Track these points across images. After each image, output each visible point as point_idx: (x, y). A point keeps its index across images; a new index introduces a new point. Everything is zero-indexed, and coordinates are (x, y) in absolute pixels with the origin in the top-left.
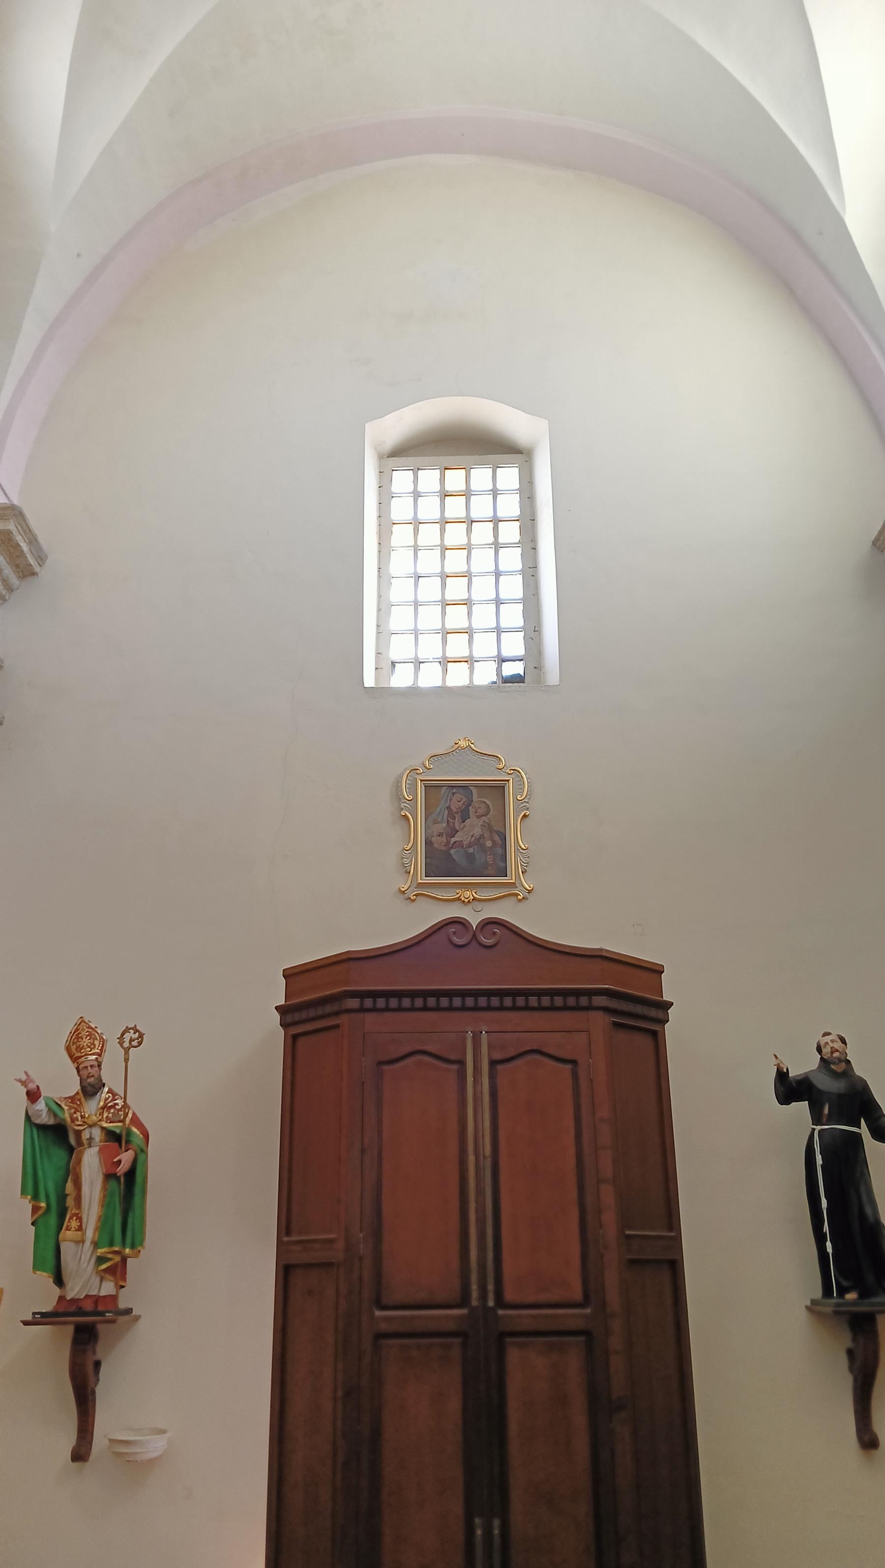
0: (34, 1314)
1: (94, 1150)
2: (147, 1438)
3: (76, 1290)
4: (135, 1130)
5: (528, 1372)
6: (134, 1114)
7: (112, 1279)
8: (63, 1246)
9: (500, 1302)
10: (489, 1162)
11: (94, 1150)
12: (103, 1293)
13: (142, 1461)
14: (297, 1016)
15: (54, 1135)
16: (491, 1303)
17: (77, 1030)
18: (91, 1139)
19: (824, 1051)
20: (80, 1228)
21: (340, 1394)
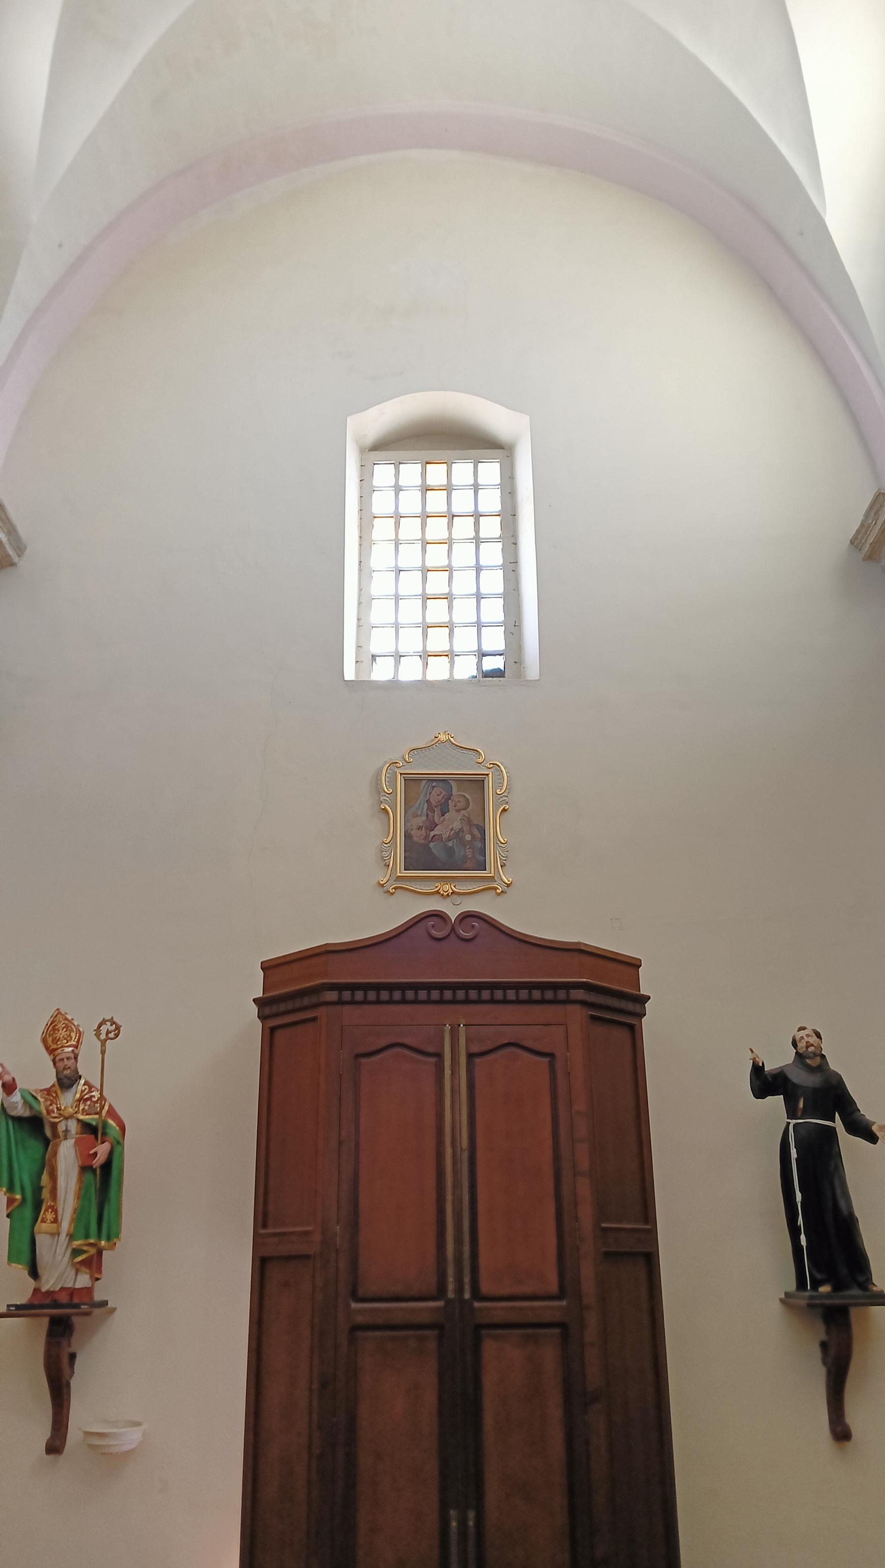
0: (8, 1306)
3: (52, 1282)
6: (110, 1106)
7: (88, 1271)
8: (39, 1239)
9: (477, 1294)
10: (465, 1156)
12: (79, 1285)
13: (117, 1453)
14: (274, 1009)
16: (467, 1296)
18: (66, 1131)
19: (800, 1045)
20: (55, 1221)
21: (315, 1386)
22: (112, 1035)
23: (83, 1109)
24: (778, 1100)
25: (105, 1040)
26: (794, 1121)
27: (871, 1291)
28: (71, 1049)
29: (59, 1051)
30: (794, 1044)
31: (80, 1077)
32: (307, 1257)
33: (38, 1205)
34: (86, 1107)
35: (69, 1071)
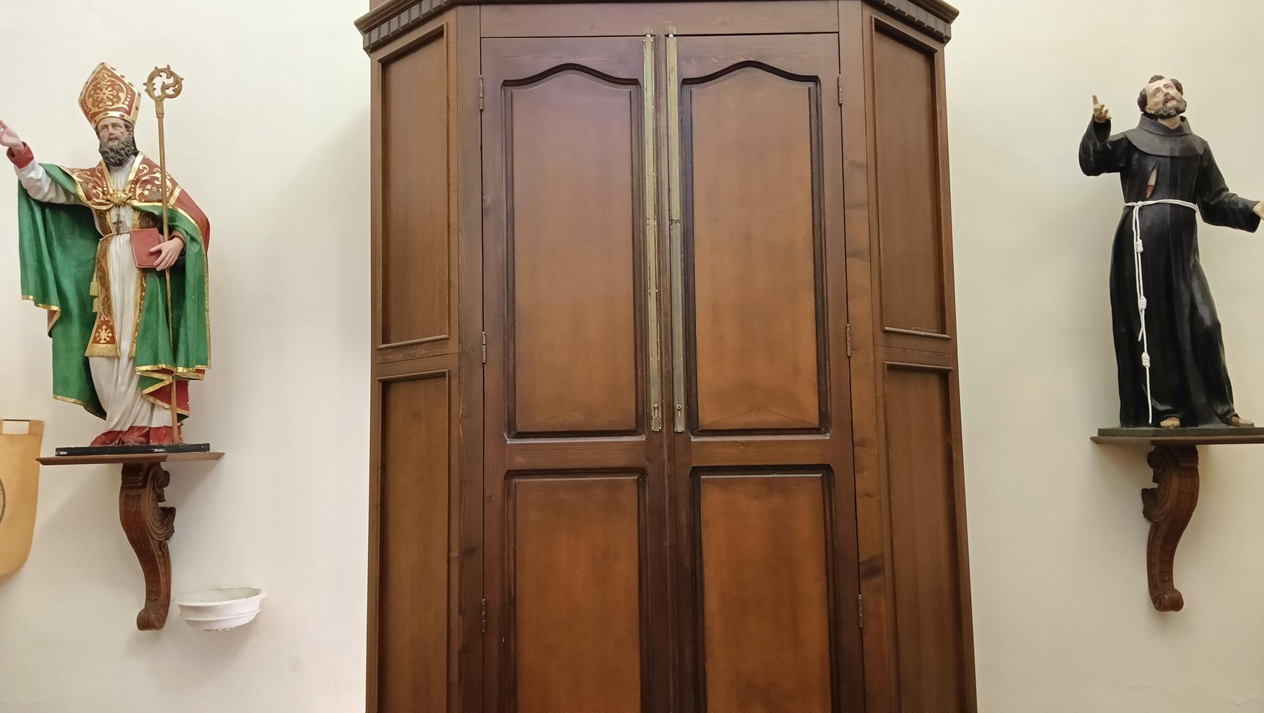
0: (58, 450)
1: (125, 238)
2: (224, 603)
3: (116, 420)
4: (180, 211)
5: (733, 523)
6: (183, 192)
7: (167, 406)
8: (93, 363)
9: (693, 425)
10: (677, 230)
11: (125, 238)
12: (155, 424)
13: (224, 630)
14: (384, 30)
15: (64, 219)
16: (680, 428)
17: (95, 79)
18: (118, 223)
19: (1150, 102)
20: (112, 340)
21: (455, 554)
22: (170, 92)
23: (142, 194)
24: (1112, 180)
25: (162, 100)
26: (1140, 203)
27: (1237, 424)
28: (117, 114)
29: (101, 116)
30: (1143, 102)
31: (136, 154)
32: (443, 375)
33: (88, 321)
34: (146, 193)
35: (116, 143)
